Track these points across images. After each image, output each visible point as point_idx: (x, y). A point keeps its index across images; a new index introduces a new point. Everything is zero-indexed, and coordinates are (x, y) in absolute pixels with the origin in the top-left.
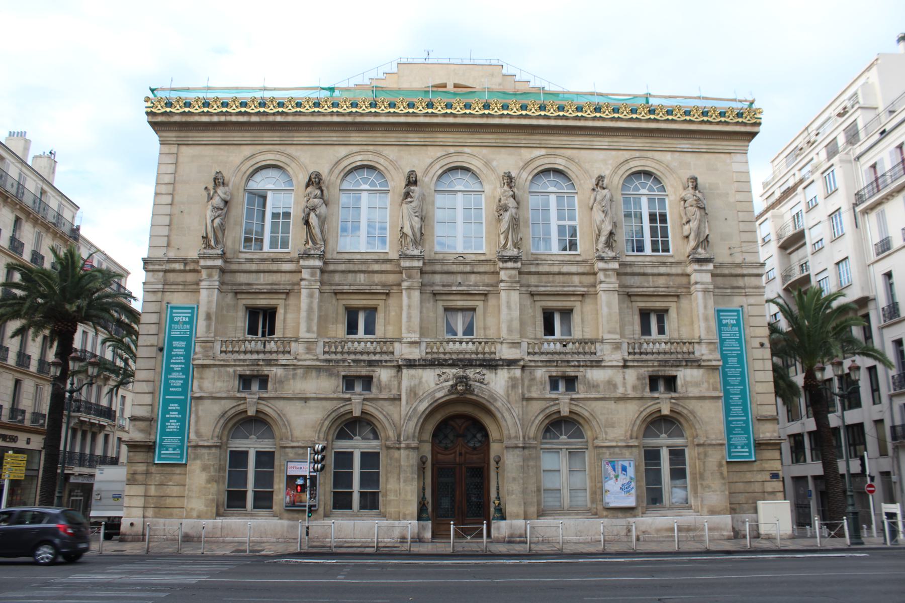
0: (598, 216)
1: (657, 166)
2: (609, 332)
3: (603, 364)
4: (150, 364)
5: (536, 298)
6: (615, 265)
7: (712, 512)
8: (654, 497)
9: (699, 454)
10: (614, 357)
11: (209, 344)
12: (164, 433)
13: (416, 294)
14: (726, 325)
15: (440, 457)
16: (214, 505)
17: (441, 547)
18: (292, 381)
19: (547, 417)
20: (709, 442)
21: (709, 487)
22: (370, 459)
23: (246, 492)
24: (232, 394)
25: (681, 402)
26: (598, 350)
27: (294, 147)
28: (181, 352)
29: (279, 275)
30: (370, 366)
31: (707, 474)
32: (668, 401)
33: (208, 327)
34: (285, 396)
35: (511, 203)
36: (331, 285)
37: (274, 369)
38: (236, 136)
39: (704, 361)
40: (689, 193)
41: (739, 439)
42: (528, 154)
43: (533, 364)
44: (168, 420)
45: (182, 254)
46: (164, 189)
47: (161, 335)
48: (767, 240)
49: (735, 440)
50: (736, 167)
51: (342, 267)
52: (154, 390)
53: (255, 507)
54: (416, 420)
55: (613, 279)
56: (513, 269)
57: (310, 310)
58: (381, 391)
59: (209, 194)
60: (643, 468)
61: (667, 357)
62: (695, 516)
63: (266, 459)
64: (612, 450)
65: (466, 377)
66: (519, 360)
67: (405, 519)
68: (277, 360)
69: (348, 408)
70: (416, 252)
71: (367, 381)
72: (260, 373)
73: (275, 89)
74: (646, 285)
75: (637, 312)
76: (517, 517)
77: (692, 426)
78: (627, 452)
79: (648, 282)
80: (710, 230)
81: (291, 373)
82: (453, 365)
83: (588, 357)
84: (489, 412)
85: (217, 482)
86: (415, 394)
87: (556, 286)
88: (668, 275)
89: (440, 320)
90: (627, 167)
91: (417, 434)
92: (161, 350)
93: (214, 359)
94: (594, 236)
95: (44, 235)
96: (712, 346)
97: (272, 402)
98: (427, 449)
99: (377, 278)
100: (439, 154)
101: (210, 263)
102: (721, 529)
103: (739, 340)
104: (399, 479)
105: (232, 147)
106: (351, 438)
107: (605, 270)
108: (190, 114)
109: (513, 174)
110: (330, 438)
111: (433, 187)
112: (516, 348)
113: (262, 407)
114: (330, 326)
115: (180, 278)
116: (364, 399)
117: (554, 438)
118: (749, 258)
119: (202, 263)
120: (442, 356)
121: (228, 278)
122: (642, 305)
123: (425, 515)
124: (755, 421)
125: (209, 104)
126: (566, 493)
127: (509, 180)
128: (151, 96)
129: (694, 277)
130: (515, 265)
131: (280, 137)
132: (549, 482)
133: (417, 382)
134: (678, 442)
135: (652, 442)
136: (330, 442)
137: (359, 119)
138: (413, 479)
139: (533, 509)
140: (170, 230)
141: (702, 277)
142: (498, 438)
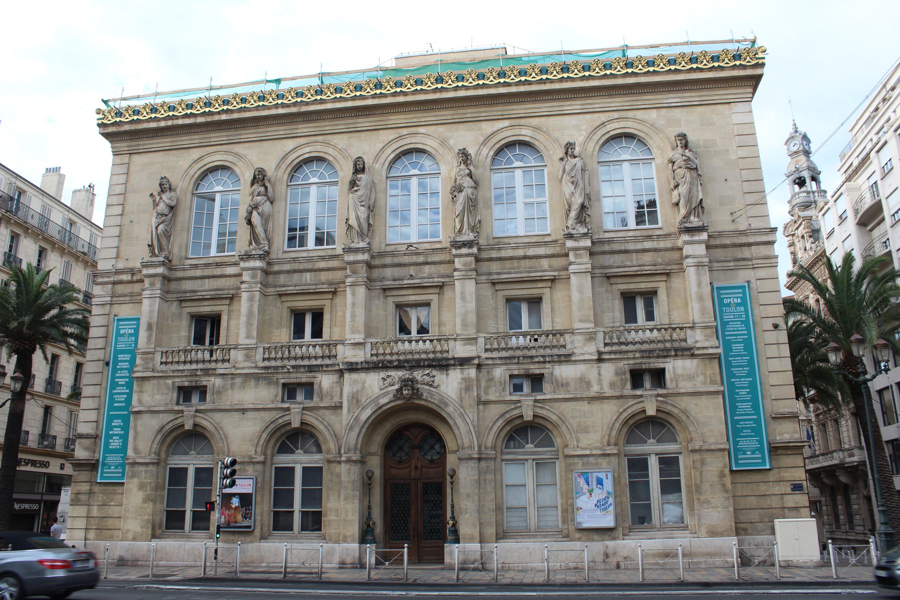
0: (568, 188)
1: (640, 127)
2: (581, 321)
3: (573, 359)
4: (96, 379)
5: (498, 287)
6: (588, 243)
7: (713, 533)
8: (640, 517)
9: (694, 462)
10: (590, 350)
11: (149, 356)
12: (108, 451)
13: (361, 291)
14: (729, 305)
15: (394, 471)
16: (150, 526)
17: (384, 573)
18: (230, 391)
19: (508, 422)
20: (707, 447)
21: (707, 502)
22: (313, 475)
23: (185, 511)
24: (170, 407)
25: (669, 400)
26: (568, 343)
27: (241, 145)
28: (126, 365)
29: (224, 280)
30: (311, 372)
31: (706, 486)
32: (653, 399)
33: (149, 337)
34: (223, 407)
35: (467, 182)
36: (275, 286)
37: (212, 379)
38: (185, 140)
39: (698, 348)
40: (677, 154)
41: (748, 443)
42: (488, 128)
43: (490, 362)
44: (111, 437)
45: (130, 265)
46: (115, 200)
47: (108, 349)
48: (844, 217)
49: (743, 443)
50: (737, 119)
51: (287, 267)
52: (99, 405)
53: (193, 529)
54: (358, 430)
55: (586, 259)
56: (468, 255)
57: (250, 314)
58: (322, 399)
59: (154, 201)
60: (625, 479)
61: (653, 346)
62: (693, 538)
63: (204, 476)
64: (585, 459)
65: (413, 380)
66: (473, 358)
67: (345, 542)
68: (215, 369)
69: (286, 418)
70: (362, 245)
71: (309, 388)
72: (199, 384)
73: (221, 88)
74: (629, 264)
75: (618, 296)
76: (471, 540)
77: (685, 429)
78: (604, 462)
79: (631, 261)
80: (703, 194)
81: (230, 382)
82: (399, 366)
83: (556, 351)
84: (444, 420)
85: (154, 502)
86: (358, 401)
87: (521, 272)
88: (656, 250)
89: (390, 318)
90: (604, 130)
91: (359, 446)
92: (107, 364)
93: (153, 370)
94: (564, 211)
95: (74, 265)
96: (708, 331)
97: (210, 414)
98: (375, 463)
99: (324, 276)
100: (391, 138)
101: (152, 271)
102: (725, 555)
103: (746, 322)
104: (339, 496)
105: (181, 151)
106: (293, 452)
107: (575, 249)
108: (139, 121)
109: (472, 151)
110: (269, 452)
111: (384, 174)
112: (471, 344)
113: (199, 420)
114: (275, 331)
115: (127, 289)
116: (304, 409)
117: (520, 448)
118: (756, 224)
119: (145, 271)
120: (388, 358)
121: (174, 286)
122: (624, 287)
123: (369, 538)
124: (769, 419)
125: (157, 110)
126: (532, 511)
127: (465, 157)
128: (103, 107)
129: (687, 250)
130: (470, 251)
131: (227, 136)
132: (512, 499)
133: (359, 387)
134: (670, 448)
135: (637, 449)
136: (269, 457)
137: (304, 109)
138: (354, 496)
139: (491, 531)
140: (120, 241)
141: (695, 250)
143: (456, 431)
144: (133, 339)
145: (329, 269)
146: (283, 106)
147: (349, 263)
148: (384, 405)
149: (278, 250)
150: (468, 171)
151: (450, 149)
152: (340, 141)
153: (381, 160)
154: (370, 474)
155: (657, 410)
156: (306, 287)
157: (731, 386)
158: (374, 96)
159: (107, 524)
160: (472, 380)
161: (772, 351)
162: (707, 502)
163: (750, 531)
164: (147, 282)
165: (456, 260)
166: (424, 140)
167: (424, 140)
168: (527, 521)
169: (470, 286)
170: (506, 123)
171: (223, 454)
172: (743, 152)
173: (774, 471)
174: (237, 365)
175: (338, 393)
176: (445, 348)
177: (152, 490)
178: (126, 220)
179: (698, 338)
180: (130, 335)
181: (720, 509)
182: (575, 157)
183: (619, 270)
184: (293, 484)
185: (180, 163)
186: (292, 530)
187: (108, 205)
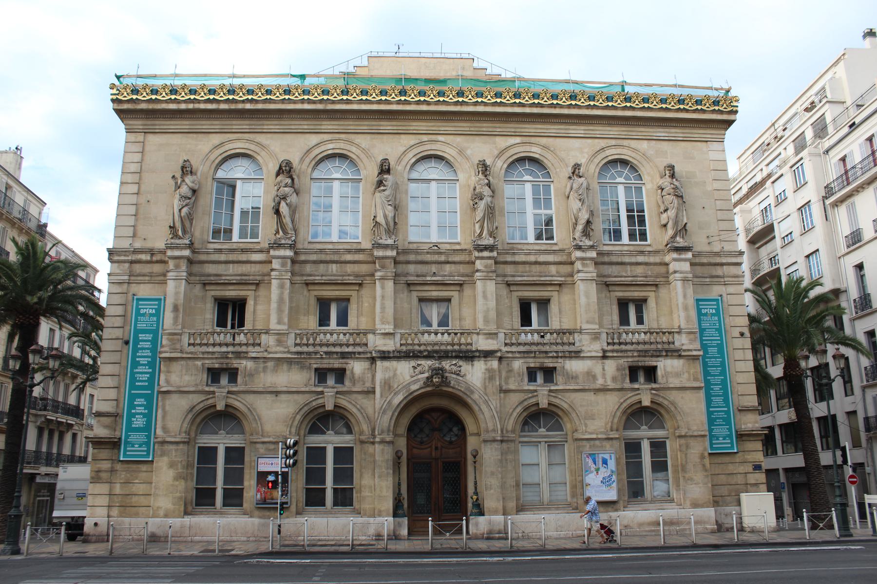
0: (575, 204)
1: (633, 155)
2: (588, 322)
4: (115, 357)
5: (513, 288)
6: (593, 254)
7: (695, 505)
8: (635, 491)
9: (680, 446)
10: (594, 348)
12: (130, 429)
13: (390, 284)
16: (182, 503)
17: (418, 544)
18: (262, 375)
20: (691, 434)
21: (691, 479)
22: (344, 455)
23: (215, 489)
24: (200, 388)
25: (661, 393)
26: (577, 341)
27: (263, 135)
28: (148, 345)
30: (343, 358)
31: (690, 466)
32: (648, 392)
33: (176, 319)
34: (256, 389)
35: (486, 191)
36: (302, 275)
37: (244, 362)
39: (685, 350)
40: (666, 182)
41: (721, 430)
42: (503, 142)
43: (510, 355)
44: (134, 415)
45: (149, 245)
46: (129, 178)
47: (127, 328)
49: (717, 431)
50: (713, 155)
51: (314, 257)
52: (120, 384)
54: (391, 414)
55: (591, 268)
56: (489, 258)
57: (281, 301)
58: (354, 384)
59: (176, 183)
61: (647, 347)
62: (677, 510)
63: (235, 455)
64: (592, 442)
67: (380, 516)
68: (247, 353)
70: (390, 242)
71: (341, 374)
73: (244, 76)
75: (616, 302)
76: (495, 512)
77: (673, 417)
78: (607, 444)
79: (626, 272)
80: (688, 219)
81: (262, 365)
82: (429, 356)
83: (566, 348)
86: (390, 387)
87: (533, 276)
88: (646, 264)
90: (603, 155)
92: (127, 343)
93: (182, 352)
95: (9, 231)
96: (692, 336)
97: (242, 396)
99: (350, 268)
100: (412, 142)
101: (177, 253)
102: (705, 523)
103: (719, 330)
106: (324, 433)
108: (157, 101)
110: (302, 432)
112: (492, 339)
113: (231, 401)
114: (302, 317)
115: (147, 269)
116: (337, 393)
118: (728, 247)
119: (169, 253)
120: (417, 348)
121: (196, 268)
122: (620, 294)
123: (400, 512)
124: (736, 411)
125: (253, 91)
126: (545, 487)
127: (484, 168)
128: (117, 83)
129: (673, 266)
130: (491, 254)
132: (527, 476)
133: (391, 374)
134: (659, 433)
135: (633, 434)
137: (330, 107)
138: (388, 473)
139: (512, 505)
140: (136, 220)
141: (680, 266)
142: (476, 431)
143: (480, 417)
144: (155, 319)
145: (354, 262)
146: (309, 101)
147: (379, 258)
148: (415, 391)
149: (305, 240)
150: (486, 181)
151: (467, 159)
152: (363, 141)
153: (403, 163)
154: (399, 454)
155: (652, 402)
156: (333, 278)
157: (707, 382)
158: (399, 102)
159: (124, 500)
160: (495, 371)
161: (739, 355)
162: (691, 479)
163: (721, 503)
164: (171, 264)
165: (478, 262)
166: (443, 148)
167: (443, 148)
168: (538, 498)
169: (491, 286)
170: (518, 140)
171: (257, 434)
172: (717, 185)
173: (740, 454)
174: (269, 349)
175: (370, 379)
176: (469, 341)
177: (183, 467)
178: (142, 199)
179: (683, 342)
180: (152, 315)
181: (701, 485)
182: (580, 177)
183: (617, 279)
184: (324, 462)
185: (200, 147)
186: (324, 505)
187: (122, 183)
